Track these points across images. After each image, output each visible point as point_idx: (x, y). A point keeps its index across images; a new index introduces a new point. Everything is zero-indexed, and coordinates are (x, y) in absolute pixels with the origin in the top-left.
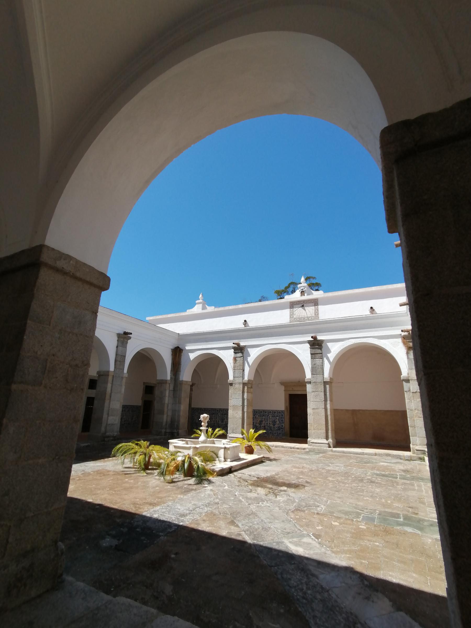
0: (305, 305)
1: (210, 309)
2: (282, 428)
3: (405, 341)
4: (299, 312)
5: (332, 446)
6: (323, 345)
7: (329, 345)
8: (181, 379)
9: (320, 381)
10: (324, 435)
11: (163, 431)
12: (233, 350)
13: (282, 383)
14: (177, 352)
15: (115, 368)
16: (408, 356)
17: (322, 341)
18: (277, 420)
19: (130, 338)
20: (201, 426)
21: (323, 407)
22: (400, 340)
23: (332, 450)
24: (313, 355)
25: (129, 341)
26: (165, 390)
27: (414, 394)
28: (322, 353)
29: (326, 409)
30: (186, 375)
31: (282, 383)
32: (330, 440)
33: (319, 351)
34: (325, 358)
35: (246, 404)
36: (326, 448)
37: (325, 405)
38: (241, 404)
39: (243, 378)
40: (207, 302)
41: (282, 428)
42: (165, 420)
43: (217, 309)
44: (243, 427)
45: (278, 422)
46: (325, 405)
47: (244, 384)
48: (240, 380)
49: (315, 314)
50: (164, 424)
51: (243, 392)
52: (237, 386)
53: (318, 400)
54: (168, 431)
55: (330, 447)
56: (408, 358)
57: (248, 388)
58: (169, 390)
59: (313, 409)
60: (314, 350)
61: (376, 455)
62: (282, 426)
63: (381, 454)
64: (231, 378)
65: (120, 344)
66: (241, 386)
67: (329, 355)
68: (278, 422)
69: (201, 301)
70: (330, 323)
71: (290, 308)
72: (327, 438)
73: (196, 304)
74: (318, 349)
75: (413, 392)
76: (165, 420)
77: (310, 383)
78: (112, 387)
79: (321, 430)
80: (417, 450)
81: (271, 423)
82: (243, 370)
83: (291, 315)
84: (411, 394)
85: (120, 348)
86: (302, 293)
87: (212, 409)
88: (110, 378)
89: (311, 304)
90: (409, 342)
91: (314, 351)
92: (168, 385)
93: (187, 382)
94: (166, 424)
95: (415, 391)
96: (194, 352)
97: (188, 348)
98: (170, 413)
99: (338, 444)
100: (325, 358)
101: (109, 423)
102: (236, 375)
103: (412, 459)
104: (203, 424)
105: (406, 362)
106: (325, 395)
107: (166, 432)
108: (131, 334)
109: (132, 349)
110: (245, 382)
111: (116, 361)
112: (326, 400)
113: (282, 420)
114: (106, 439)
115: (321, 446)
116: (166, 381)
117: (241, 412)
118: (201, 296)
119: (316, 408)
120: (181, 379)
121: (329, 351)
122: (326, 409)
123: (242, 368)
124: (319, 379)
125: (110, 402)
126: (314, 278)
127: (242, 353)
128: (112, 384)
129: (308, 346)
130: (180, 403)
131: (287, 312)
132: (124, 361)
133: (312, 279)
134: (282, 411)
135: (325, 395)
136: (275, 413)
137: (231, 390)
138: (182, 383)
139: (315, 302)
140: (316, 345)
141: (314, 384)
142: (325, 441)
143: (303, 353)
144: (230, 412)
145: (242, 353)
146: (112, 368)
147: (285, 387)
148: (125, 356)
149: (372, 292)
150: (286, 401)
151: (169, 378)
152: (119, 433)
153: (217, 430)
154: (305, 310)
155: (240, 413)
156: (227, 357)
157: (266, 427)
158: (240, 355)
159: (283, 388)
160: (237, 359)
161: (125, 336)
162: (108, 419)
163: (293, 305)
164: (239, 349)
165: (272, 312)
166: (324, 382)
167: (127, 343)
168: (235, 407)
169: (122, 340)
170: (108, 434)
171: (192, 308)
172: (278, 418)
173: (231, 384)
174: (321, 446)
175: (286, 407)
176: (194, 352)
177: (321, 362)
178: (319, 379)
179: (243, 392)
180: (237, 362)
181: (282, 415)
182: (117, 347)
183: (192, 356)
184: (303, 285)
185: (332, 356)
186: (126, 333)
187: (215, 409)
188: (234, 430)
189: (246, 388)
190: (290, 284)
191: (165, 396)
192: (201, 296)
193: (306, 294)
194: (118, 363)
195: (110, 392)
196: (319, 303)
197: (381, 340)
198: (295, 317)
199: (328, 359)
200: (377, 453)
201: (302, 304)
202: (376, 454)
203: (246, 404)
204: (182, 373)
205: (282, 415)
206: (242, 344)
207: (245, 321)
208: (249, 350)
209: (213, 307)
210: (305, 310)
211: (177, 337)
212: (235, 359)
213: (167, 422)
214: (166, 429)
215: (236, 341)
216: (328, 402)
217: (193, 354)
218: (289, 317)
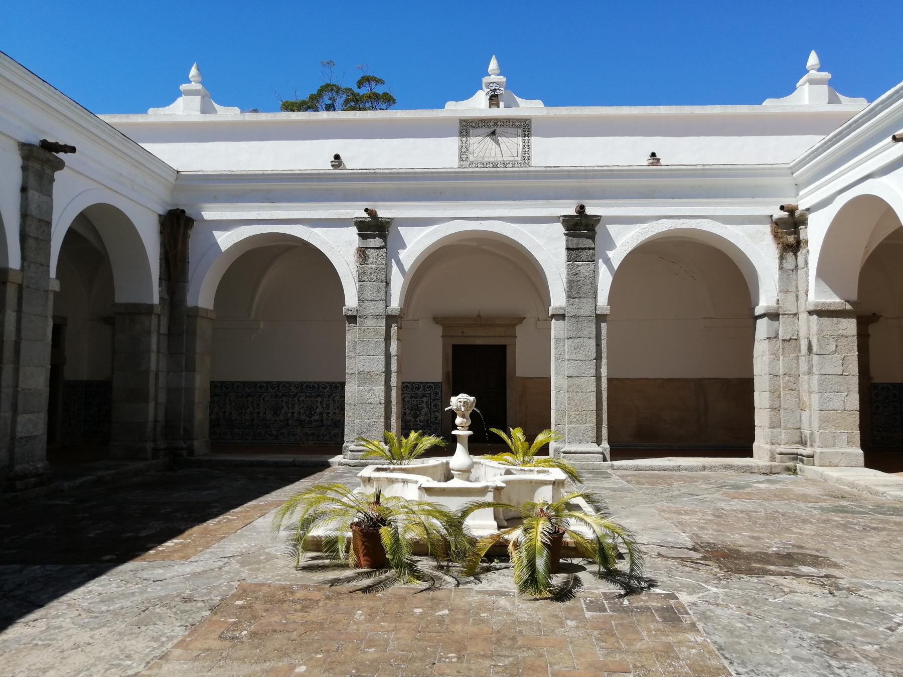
0: (498, 130)
1: (228, 114)
2: (434, 423)
3: (779, 231)
4: (483, 148)
5: (608, 456)
6: (597, 229)
7: (612, 229)
8: (190, 303)
9: (589, 313)
10: (594, 434)
11: (149, 446)
12: (354, 230)
13: (438, 320)
14: (177, 225)
15: (23, 258)
16: (781, 263)
17: (597, 219)
18: (425, 405)
19: (60, 165)
20: (455, 427)
21: (593, 371)
22: (767, 229)
23: (612, 466)
24: (572, 252)
25: (58, 175)
26: (149, 333)
27: (786, 344)
28: (593, 249)
29: (598, 378)
30: (202, 294)
31: (438, 320)
32: (605, 445)
33: (588, 243)
34: (601, 261)
35: (394, 367)
36: (598, 462)
37: (598, 367)
38: (382, 367)
39: (387, 300)
40: (216, 92)
41: (434, 423)
42: (151, 417)
43: (249, 117)
44: (387, 427)
45: (425, 410)
46: (598, 367)
47: (390, 319)
48: (380, 308)
49: (523, 157)
50: (150, 425)
51: (388, 338)
52: (370, 322)
53: (580, 356)
54: (162, 444)
55: (605, 460)
56: (781, 268)
57: (399, 328)
58: (159, 334)
59: (569, 377)
60: (575, 240)
61: (704, 470)
62: (436, 418)
63: (715, 466)
64: (351, 301)
65: (32, 181)
66: (383, 322)
67: (610, 254)
68: (425, 410)
69: (195, 86)
70: (627, 176)
71: (461, 135)
72: (598, 442)
73: (179, 94)
74: (587, 237)
75: (784, 340)
76: (151, 417)
77: (562, 317)
78: (19, 321)
79: (585, 423)
80: (781, 454)
81: (302, 411)
82: (388, 284)
83: (463, 153)
84: (780, 343)
85: (33, 194)
86: (494, 99)
87: (245, 384)
88: (11, 293)
89: (515, 131)
90: (787, 233)
91: (575, 242)
92: (154, 320)
93: (207, 310)
94: (155, 429)
95: (788, 338)
96: (229, 228)
97: (210, 214)
98: (162, 398)
99: (619, 451)
100: (601, 261)
101: (19, 435)
102: (367, 295)
103: (774, 471)
104: (458, 420)
105: (777, 276)
106: (598, 345)
107: (156, 450)
108: (73, 150)
109: (69, 198)
110: (394, 313)
111: (23, 237)
112: (598, 358)
113: (435, 405)
114: (18, 484)
115: (588, 459)
116: (151, 306)
117: (382, 388)
118: (193, 71)
119: (575, 374)
120: (190, 303)
121: (611, 245)
122: (598, 378)
123: (383, 278)
124: (586, 308)
125: (16, 371)
126: (379, 81)
127: (384, 237)
128: (19, 311)
129: (559, 229)
130: (191, 368)
131: (452, 144)
132: (47, 240)
133: (373, 84)
134: (436, 384)
135: (598, 345)
136: (418, 388)
137: (352, 334)
138: (195, 312)
139: (524, 127)
140: (582, 228)
141: (573, 320)
142: (594, 447)
143: (548, 248)
144: (351, 390)
145: (384, 237)
146: (14, 261)
147: (445, 328)
148: (49, 224)
149: (882, 102)
150: (445, 359)
151: (156, 300)
152: (46, 462)
153: (413, 435)
154: (498, 143)
155: (379, 391)
156: (340, 247)
157: (290, 422)
158: (377, 242)
159: (439, 331)
160: (368, 252)
161: (46, 155)
162: (14, 421)
163: (467, 127)
164: (374, 228)
165: (412, 140)
166: (597, 316)
167: (52, 180)
168: (365, 377)
169: (37, 166)
170: (18, 468)
171: (164, 106)
172: (425, 399)
173: (353, 319)
174: (588, 459)
175: (446, 375)
176: (229, 228)
177: (592, 268)
178: (586, 308)
179: (388, 338)
180: (369, 261)
181: (437, 393)
182: (24, 190)
183: (225, 240)
184: (493, 78)
185: (617, 256)
186: (50, 147)
187: (255, 384)
188: (362, 433)
189: (394, 329)
190: (327, 85)
191: (149, 351)
192: (193, 71)
193: (502, 104)
194: (31, 243)
195: (13, 338)
196: (533, 130)
197: (728, 226)
198: (471, 158)
199: (607, 262)
200: (706, 464)
201: (492, 128)
202: (704, 468)
203: (394, 367)
204: (191, 288)
205: (437, 393)
206: (383, 213)
207: (337, 157)
208: (402, 230)
209: (237, 110)
210: (498, 143)
211: (172, 180)
212: (362, 253)
213: (156, 421)
214: (154, 441)
215: (369, 205)
216: (604, 362)
217: (227, 234)
218: (457, 159)
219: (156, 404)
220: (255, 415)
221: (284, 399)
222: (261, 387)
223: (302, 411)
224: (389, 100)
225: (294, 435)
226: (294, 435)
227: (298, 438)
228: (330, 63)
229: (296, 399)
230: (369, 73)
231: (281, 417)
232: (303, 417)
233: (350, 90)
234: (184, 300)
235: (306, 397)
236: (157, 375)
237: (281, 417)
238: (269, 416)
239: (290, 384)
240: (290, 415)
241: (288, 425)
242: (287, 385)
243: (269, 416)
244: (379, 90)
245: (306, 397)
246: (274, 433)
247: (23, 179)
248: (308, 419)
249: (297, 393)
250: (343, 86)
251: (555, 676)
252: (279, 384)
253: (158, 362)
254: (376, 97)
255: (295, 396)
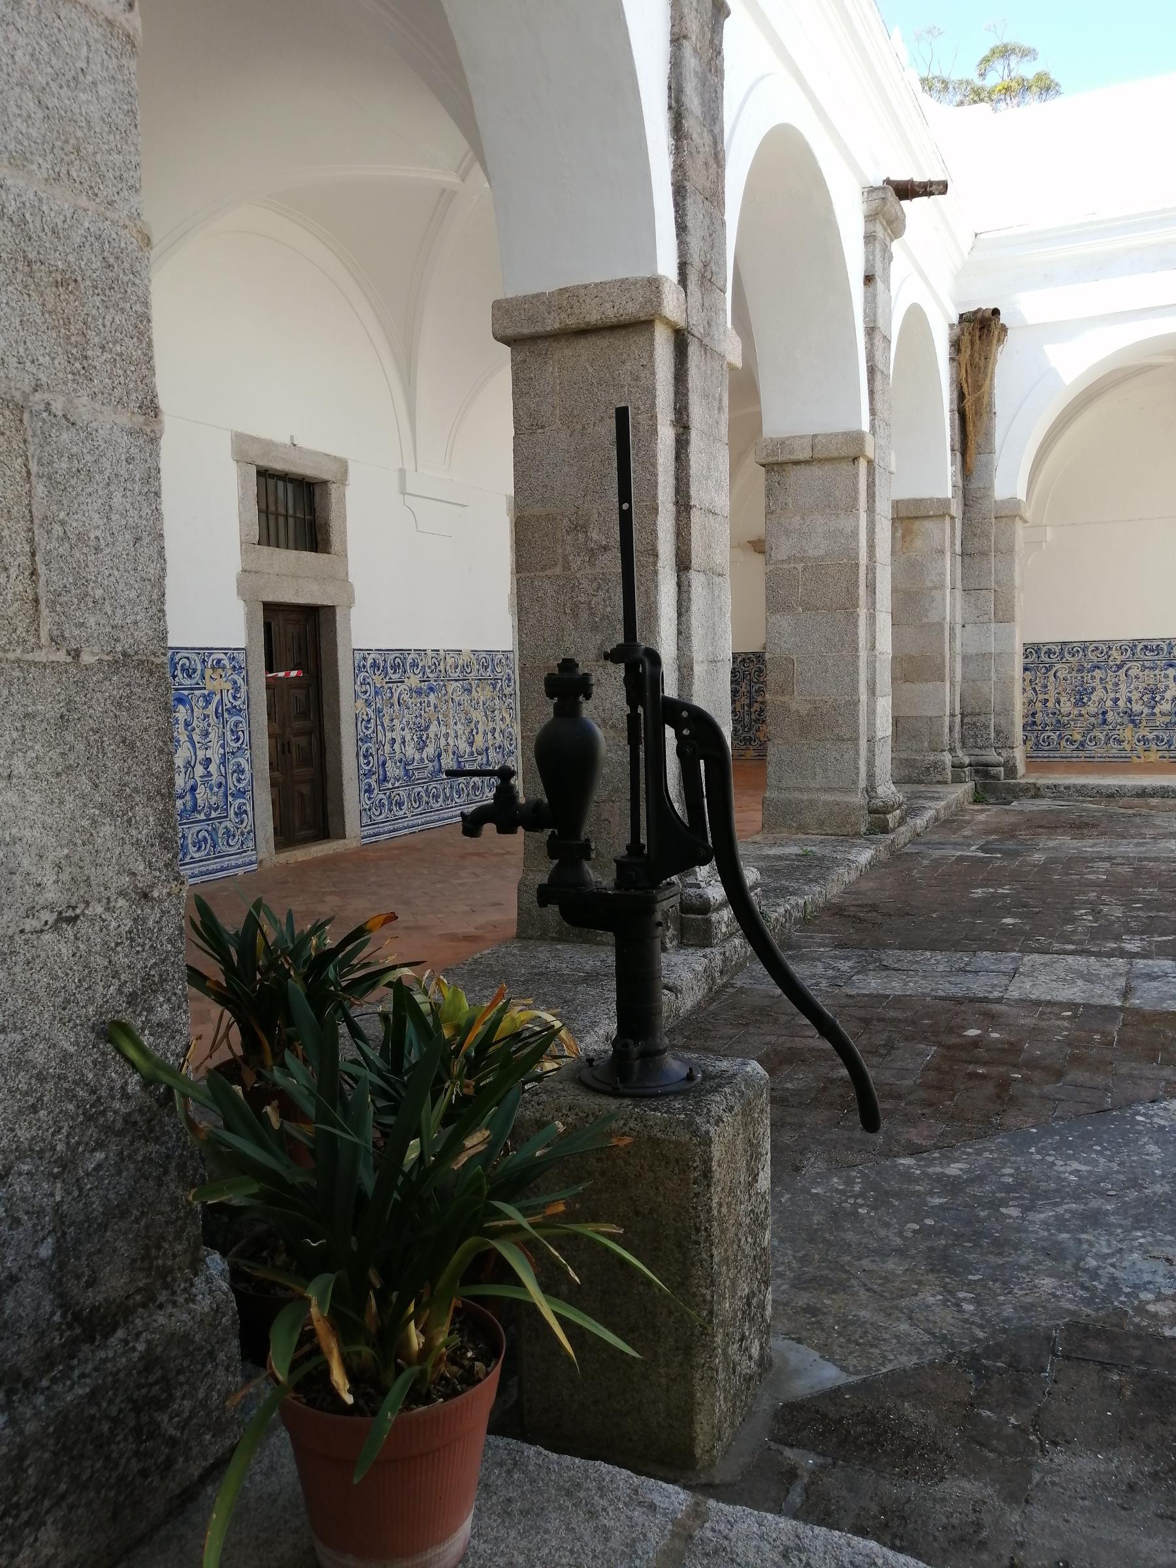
11: (947, 758)
58: (953, 553)
81: (1135, 696)
126: (1026, 53)
157: (1110, 716)
214: (952, 750)
219: (952, 684)
220: (1039, 705)
221: (1098, 673)
222: (1049, 653)
223: (1135, 696)
224: (1048, 89)
225: (1120, 742)
226: (1120, 742)
227: (1128, 747)
228: (933, 32)
229: (1122, 672)
230: (1010, 37)
231: (1092, 708)
232: (1137, 707)
233: (967, 82)
234: (989, 488)
235: (1144, 668)
236: (952, 629)
237: (1092, 708)
238: (1066, 707)
239: (1109, 645)
240: (1109, 703)
241: (1105, 722)
242: (1103, 648)
243: (1066, 707)
244: (1027, 70)
245: (1144, 668)
246: (1078, 737)
247: (867, 260)
248: (1146, 711)
249: (1123, 663)
250: (955, 77)
251: (1174, 1191)
252: (1084, 646)
253: (953, 606)
254: (1024, 87)
255: (1120, 667)
